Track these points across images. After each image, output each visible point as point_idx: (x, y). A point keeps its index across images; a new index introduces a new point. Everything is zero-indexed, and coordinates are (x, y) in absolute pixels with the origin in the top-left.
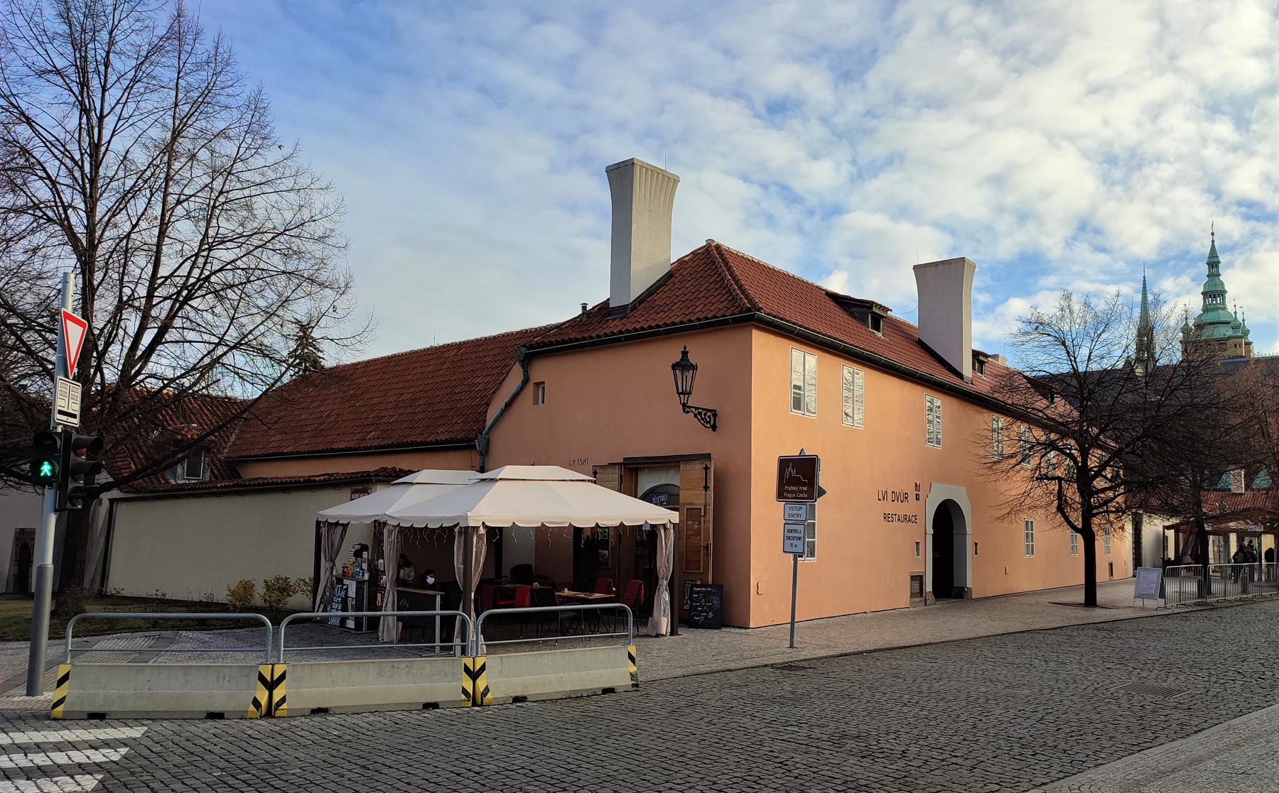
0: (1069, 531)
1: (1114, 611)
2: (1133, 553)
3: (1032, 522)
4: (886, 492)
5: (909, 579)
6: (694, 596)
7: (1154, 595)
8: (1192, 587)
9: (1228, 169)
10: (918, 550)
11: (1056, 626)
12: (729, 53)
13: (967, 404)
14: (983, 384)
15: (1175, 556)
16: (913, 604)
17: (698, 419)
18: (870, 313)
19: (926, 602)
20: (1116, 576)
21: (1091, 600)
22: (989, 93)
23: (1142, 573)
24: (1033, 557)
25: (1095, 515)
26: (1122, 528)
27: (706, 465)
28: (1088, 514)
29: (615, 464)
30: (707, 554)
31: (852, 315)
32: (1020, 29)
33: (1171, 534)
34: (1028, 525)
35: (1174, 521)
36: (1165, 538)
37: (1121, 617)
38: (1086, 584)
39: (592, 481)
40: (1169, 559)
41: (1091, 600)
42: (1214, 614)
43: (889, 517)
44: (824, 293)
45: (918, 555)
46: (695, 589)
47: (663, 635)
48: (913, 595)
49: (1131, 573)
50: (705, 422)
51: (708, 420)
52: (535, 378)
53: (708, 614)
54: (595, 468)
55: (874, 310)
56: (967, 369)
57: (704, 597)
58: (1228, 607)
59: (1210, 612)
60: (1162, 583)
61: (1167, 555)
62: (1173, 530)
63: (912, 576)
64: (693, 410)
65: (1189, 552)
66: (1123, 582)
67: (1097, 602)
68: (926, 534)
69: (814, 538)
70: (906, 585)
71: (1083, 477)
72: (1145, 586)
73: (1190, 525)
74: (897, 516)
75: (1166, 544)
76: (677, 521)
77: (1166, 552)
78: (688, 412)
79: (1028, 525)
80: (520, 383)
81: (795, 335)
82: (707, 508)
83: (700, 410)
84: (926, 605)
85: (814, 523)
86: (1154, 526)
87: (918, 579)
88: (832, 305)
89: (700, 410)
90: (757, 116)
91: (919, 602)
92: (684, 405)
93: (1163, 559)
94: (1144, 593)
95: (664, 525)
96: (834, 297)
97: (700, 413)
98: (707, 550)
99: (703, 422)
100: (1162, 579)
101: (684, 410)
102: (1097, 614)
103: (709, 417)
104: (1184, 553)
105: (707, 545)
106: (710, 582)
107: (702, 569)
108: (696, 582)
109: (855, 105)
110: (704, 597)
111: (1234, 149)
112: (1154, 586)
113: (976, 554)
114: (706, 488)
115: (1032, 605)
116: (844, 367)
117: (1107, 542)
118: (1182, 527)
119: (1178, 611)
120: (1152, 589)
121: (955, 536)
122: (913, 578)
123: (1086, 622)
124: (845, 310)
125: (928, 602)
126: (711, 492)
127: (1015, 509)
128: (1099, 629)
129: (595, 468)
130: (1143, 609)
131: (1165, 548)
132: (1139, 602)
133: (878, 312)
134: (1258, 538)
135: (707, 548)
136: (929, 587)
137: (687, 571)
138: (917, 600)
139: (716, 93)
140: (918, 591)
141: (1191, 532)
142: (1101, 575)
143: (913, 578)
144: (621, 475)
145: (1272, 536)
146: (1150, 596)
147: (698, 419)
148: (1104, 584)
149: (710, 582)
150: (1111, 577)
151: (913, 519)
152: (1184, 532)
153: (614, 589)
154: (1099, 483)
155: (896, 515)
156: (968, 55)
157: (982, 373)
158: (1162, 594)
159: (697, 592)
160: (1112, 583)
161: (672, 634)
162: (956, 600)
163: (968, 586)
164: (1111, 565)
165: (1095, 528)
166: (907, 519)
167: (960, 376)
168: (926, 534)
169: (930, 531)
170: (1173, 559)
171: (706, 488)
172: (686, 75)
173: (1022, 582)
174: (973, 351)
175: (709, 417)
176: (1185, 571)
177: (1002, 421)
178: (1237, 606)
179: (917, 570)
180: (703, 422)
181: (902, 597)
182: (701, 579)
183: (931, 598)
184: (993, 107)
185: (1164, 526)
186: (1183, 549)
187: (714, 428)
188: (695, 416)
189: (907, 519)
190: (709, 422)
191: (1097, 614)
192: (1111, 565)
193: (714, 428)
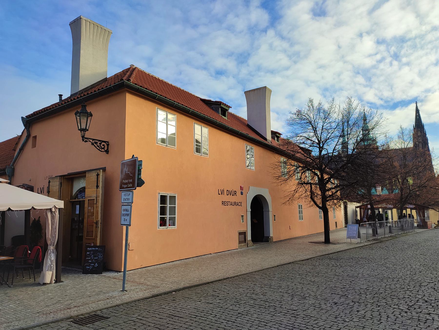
0: (318, 209)
1: (338, 246)
2: (344, 218)
3: (301, 205)
4: (223, 190)
5: (237, 234)
6: (88, 253)
7: (355, 237)
8: (370, 231)
9: (364, 93)
10: (243, 219)
11: (309, 257)
12: (202, 54)
13: (268, 151)
14: (275, 143)
15: (360, 218)
16: (240, 247)
17: (95, 146)
18: (220, 107)
19: (248, 246)
20: (338, 227)
21: (327, 241)
22: (287, 69)
23: (350, 227)
24: (303, 221)
25: (328, 201)
26: (340, 206)
27: (98, 173)
28: (325, 199)
29: (58, 176)
30: (97, 227)
31: (212, 109)
32: (297, 48)
33: (358, 209)
34: (300, 207)
35: (358, 205)
36: (356, 211)
37: (341, 250)
38: (325, 232)
39: (6, 183)
40: (358, 220)
41: (327, 241)
42: (383, 245)
43: (225, 203)
44: (200, 99)
45: (243, 222)
46: (88, 249)
47: (45, 284)
48: (240, 242)
49: (344, 226)
50: (100, 149)
51: (103, 147)
52: (33, 134)
53: (94, 265)
54: (49, 179)
55: (222, 106)
56: (269, 137)
57: (93, 254)
58: (387, 241)
59: (381, 244)
60: (359, 231)
61: (357, 218)
62: (359, 208)
63: (239, 233)
64: (91, 140)
65: (365, 217)
66: (341, 230)
67: (330, 240)
68: (247, 211)
69: (175, 215)
70: (236, 237)
71: (322, 183)
72: (351, 233)
73: (365, 206)
74: (230, 203)
75: (357, 214)
76: (62, 206)
77: (357, 217)
78: (86, 141)
79: (300, 207)
80: (26, 137)
81: (156, 100)
82: (98, 198)
83: (96, 141)
84: (248, 247)
85: (175, 207)
86: (352, 206)
87: (243, 234)
88: (202, 103)
89: (96, 141)
90: (211, 76)
91: (244, 245)
92: (83, 137)
93: (356, 220)
94: (351, 236)
95: (51, 209)
96: (204, 101)
97: (96, 143)
98: (97, 225)
99: (99, 148)
100: (359, 229)
101: (83, 140)
102: (331, 248)
103: (103, 145)
104: (364, 217)
105: (97, 221)
106: (98, 244)
107: (94, 236)
108: (91, 244)
109: (244, 71)
110: (93, 254)
111: (366, 86)
112: (355, 232)
113: (275, 220)
114: (97, 187)
115: (300, 244)
116: (195, 124)
117: (334, 213)
118: (363, 207)
119: (366, 244)
120: (354, 234)
121: (264, 212)
122: (240, 234)
123: (324, 253)
124: (209, 107)
125: (249, 245)
126: (100, 190)
127: (291, 199)
128: (330, 259)
129: (49, 179)
130: (351, 243)
131: (356, 215)
132: (349, 240)
133: (224, 107)
134: (391, 210)
135: (97, 223)
136: (249, 237)
137: (88, 238)
138: (243, 244)
139: (197, 68)
140: (243, 240)
141: (366, 209)
142: (332, 227)
143: (240, 234)
144: (61, 183)
145: (396, 209)
146: (354, 238)
147: (95, 146)
148: (334, 231)
149: (98, 244)
150: (336, 228)
151: (240, 204)
152: (363, 209)
153: (29, 252)
154: (329, 186)
155: (229, 202)
156: (281, 56)
157: (278, 142)
158: (359, 237)
159: (90, 251)
160: (337, 231)
161: (56, 282)
162: (265, 243)
163: (271, 236)
164: (336, 223)
165: (328, 207)
166: (236, 204)
167: (266, 139)
168: (247, 211)
169: (249, 210)
170: (359, 219)
171: (97, 187)
172: (188, 62)
173: (297, 232)
174: (272, 131)
175: (103, 145)
176: (368, 225)
177: (283, 159)
178: (390, 239)
179: (242, 230)
180: (99, 148)
181: (234, 244)
182: (93, 243)
183: (251, 243)
184: (289, 72)
185: (355, 207)
186: (363, 216)
187: (107, 152)
188: (93, 144)
189: (236, 204)
190: (104, 148)
191: (331, 248)
192: (336, 223)
193: (107, 152)
